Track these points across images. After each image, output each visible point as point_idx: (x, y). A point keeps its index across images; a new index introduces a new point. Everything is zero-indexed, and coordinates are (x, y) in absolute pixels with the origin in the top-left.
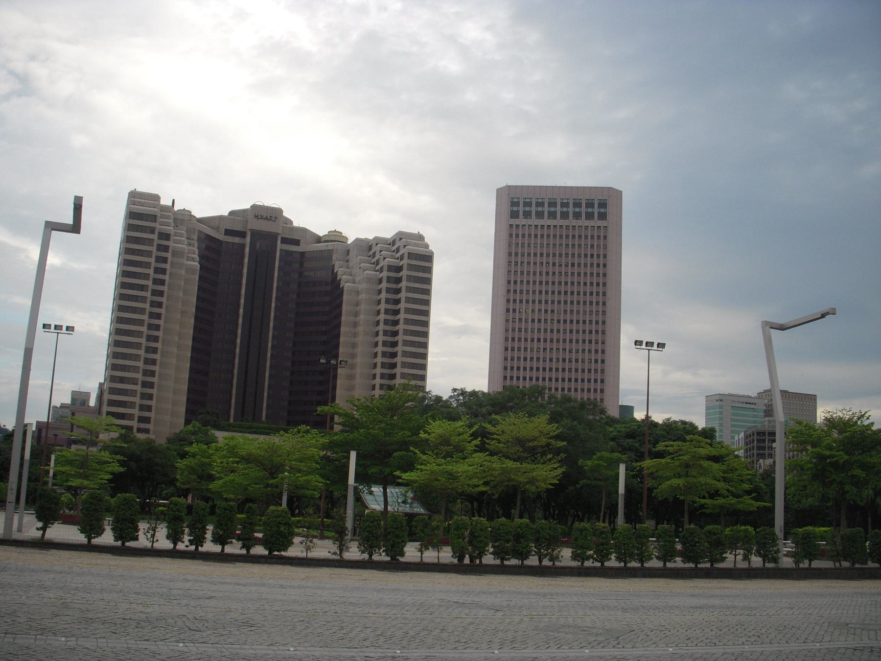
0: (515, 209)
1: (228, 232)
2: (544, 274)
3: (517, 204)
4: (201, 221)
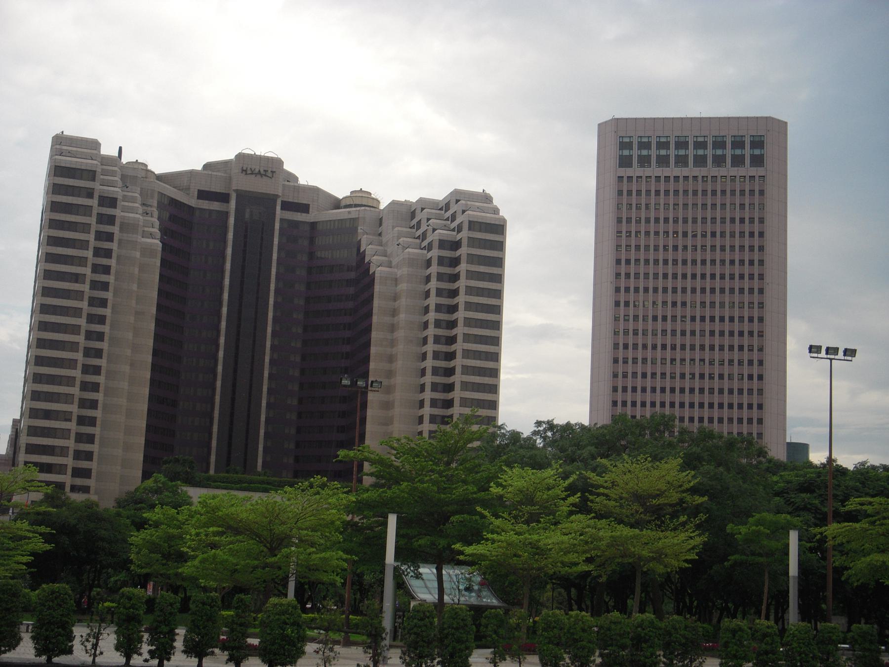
0: (626, 152)
1: (203, 195)
3: (629, 146)
4: (161, 178)
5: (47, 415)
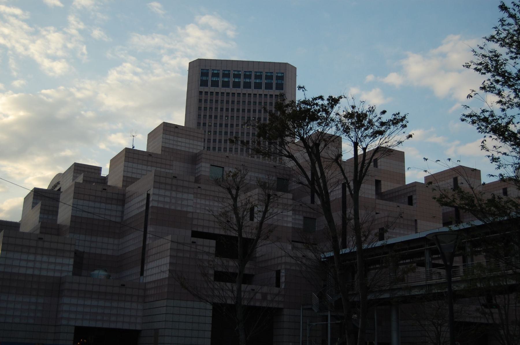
0: (204, 78)
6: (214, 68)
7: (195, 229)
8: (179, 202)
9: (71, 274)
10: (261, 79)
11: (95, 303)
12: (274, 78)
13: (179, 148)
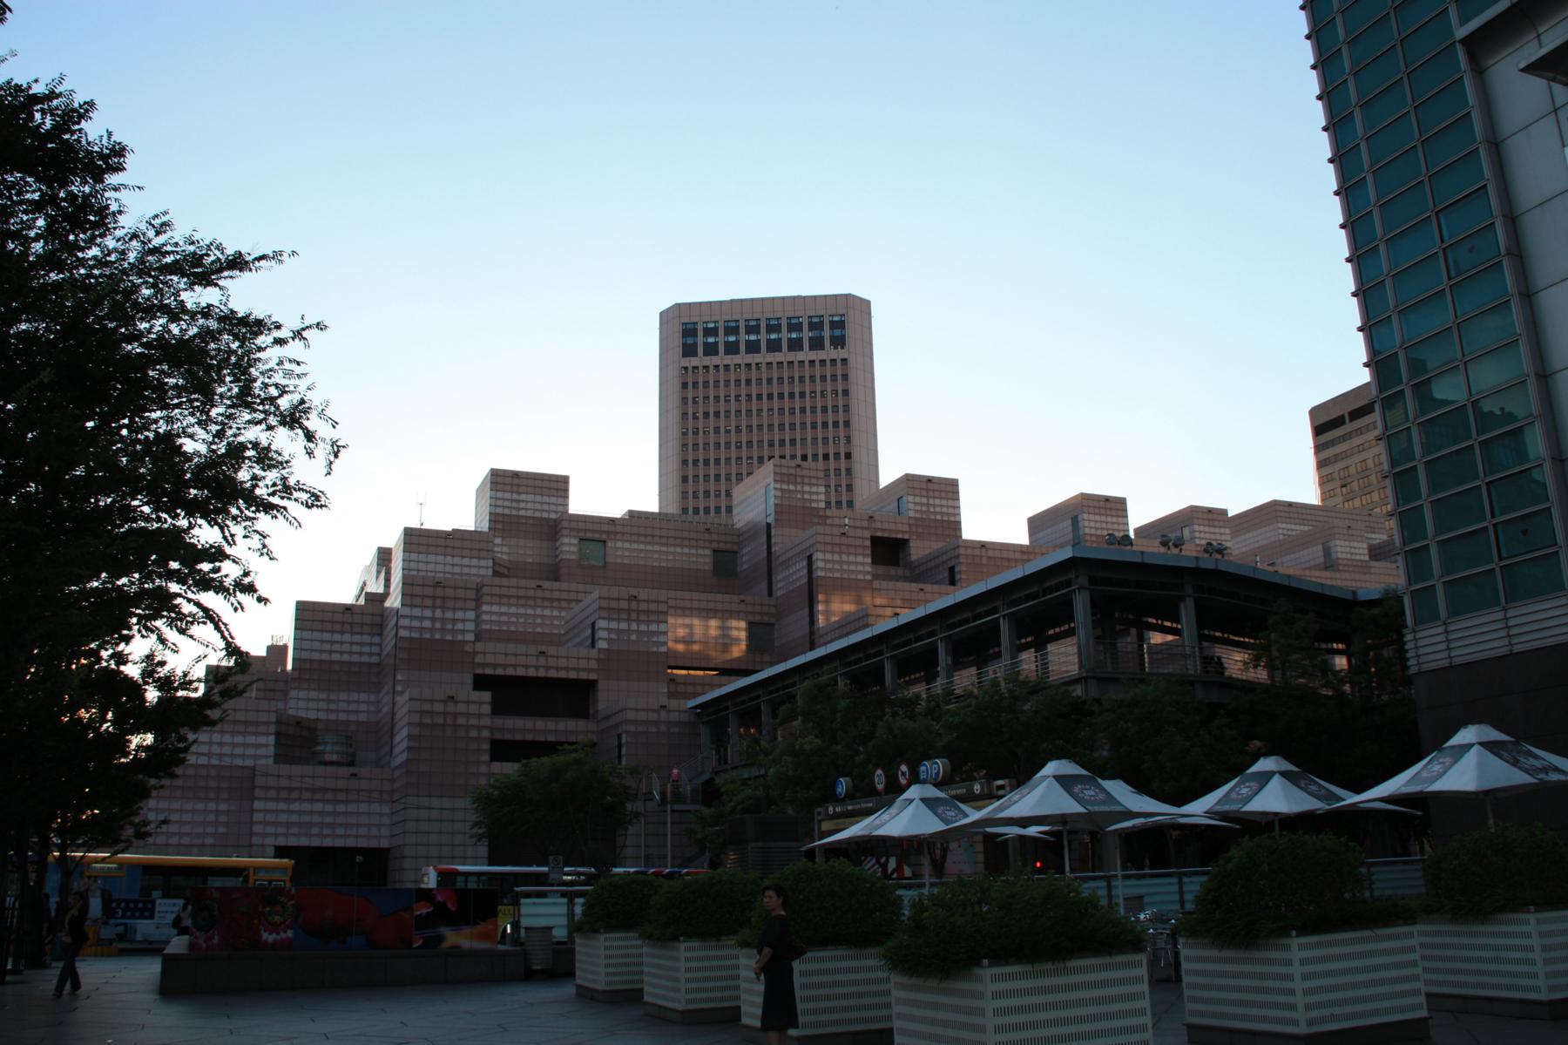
0: (690, 341)
2: (701, 495)
5: (635, 964)
6: (707, 319)
7: (479, 671)
8: (449, 626)
9: (271, 761)
10: (801, 330)
11: (306, 806)
12: (827, 326)
13: (522, 513)
